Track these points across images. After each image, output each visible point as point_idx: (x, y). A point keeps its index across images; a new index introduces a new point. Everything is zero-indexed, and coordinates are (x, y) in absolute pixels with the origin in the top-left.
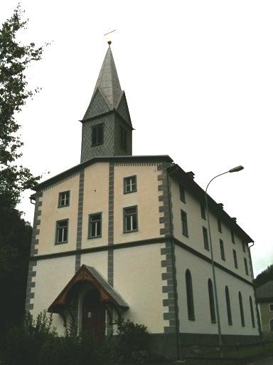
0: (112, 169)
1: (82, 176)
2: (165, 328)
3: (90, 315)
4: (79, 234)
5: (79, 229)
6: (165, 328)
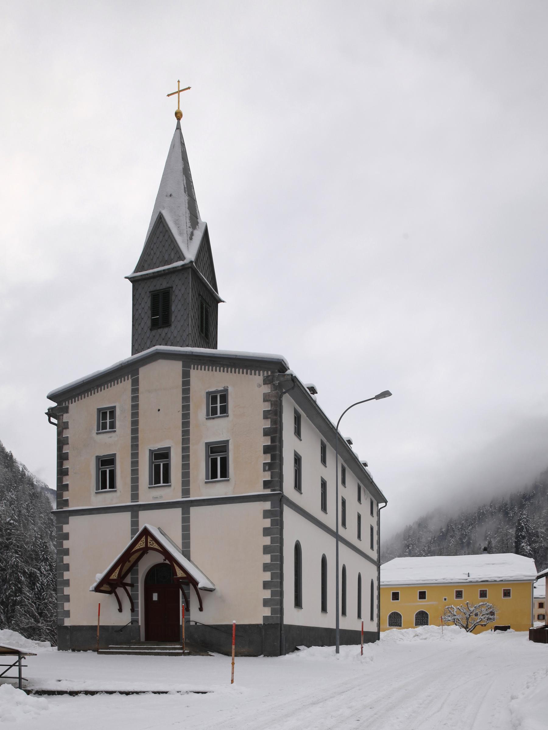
0: (186, 375)
1: (135, 382)
2: (265, 618)
3: (155, 597)
4: (135, 480)
5: (135, 472)
6: (265, 618)
